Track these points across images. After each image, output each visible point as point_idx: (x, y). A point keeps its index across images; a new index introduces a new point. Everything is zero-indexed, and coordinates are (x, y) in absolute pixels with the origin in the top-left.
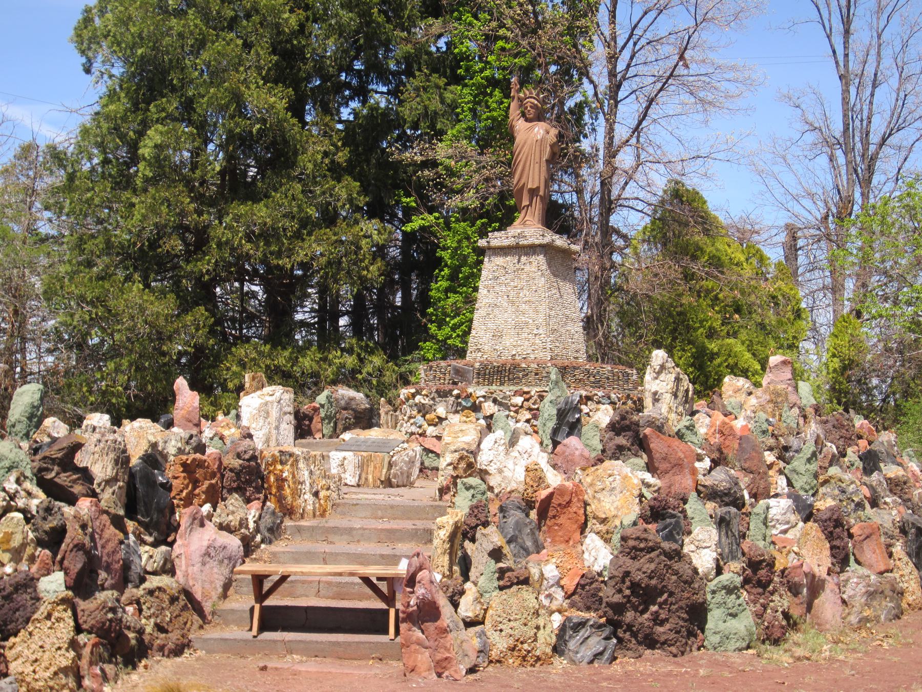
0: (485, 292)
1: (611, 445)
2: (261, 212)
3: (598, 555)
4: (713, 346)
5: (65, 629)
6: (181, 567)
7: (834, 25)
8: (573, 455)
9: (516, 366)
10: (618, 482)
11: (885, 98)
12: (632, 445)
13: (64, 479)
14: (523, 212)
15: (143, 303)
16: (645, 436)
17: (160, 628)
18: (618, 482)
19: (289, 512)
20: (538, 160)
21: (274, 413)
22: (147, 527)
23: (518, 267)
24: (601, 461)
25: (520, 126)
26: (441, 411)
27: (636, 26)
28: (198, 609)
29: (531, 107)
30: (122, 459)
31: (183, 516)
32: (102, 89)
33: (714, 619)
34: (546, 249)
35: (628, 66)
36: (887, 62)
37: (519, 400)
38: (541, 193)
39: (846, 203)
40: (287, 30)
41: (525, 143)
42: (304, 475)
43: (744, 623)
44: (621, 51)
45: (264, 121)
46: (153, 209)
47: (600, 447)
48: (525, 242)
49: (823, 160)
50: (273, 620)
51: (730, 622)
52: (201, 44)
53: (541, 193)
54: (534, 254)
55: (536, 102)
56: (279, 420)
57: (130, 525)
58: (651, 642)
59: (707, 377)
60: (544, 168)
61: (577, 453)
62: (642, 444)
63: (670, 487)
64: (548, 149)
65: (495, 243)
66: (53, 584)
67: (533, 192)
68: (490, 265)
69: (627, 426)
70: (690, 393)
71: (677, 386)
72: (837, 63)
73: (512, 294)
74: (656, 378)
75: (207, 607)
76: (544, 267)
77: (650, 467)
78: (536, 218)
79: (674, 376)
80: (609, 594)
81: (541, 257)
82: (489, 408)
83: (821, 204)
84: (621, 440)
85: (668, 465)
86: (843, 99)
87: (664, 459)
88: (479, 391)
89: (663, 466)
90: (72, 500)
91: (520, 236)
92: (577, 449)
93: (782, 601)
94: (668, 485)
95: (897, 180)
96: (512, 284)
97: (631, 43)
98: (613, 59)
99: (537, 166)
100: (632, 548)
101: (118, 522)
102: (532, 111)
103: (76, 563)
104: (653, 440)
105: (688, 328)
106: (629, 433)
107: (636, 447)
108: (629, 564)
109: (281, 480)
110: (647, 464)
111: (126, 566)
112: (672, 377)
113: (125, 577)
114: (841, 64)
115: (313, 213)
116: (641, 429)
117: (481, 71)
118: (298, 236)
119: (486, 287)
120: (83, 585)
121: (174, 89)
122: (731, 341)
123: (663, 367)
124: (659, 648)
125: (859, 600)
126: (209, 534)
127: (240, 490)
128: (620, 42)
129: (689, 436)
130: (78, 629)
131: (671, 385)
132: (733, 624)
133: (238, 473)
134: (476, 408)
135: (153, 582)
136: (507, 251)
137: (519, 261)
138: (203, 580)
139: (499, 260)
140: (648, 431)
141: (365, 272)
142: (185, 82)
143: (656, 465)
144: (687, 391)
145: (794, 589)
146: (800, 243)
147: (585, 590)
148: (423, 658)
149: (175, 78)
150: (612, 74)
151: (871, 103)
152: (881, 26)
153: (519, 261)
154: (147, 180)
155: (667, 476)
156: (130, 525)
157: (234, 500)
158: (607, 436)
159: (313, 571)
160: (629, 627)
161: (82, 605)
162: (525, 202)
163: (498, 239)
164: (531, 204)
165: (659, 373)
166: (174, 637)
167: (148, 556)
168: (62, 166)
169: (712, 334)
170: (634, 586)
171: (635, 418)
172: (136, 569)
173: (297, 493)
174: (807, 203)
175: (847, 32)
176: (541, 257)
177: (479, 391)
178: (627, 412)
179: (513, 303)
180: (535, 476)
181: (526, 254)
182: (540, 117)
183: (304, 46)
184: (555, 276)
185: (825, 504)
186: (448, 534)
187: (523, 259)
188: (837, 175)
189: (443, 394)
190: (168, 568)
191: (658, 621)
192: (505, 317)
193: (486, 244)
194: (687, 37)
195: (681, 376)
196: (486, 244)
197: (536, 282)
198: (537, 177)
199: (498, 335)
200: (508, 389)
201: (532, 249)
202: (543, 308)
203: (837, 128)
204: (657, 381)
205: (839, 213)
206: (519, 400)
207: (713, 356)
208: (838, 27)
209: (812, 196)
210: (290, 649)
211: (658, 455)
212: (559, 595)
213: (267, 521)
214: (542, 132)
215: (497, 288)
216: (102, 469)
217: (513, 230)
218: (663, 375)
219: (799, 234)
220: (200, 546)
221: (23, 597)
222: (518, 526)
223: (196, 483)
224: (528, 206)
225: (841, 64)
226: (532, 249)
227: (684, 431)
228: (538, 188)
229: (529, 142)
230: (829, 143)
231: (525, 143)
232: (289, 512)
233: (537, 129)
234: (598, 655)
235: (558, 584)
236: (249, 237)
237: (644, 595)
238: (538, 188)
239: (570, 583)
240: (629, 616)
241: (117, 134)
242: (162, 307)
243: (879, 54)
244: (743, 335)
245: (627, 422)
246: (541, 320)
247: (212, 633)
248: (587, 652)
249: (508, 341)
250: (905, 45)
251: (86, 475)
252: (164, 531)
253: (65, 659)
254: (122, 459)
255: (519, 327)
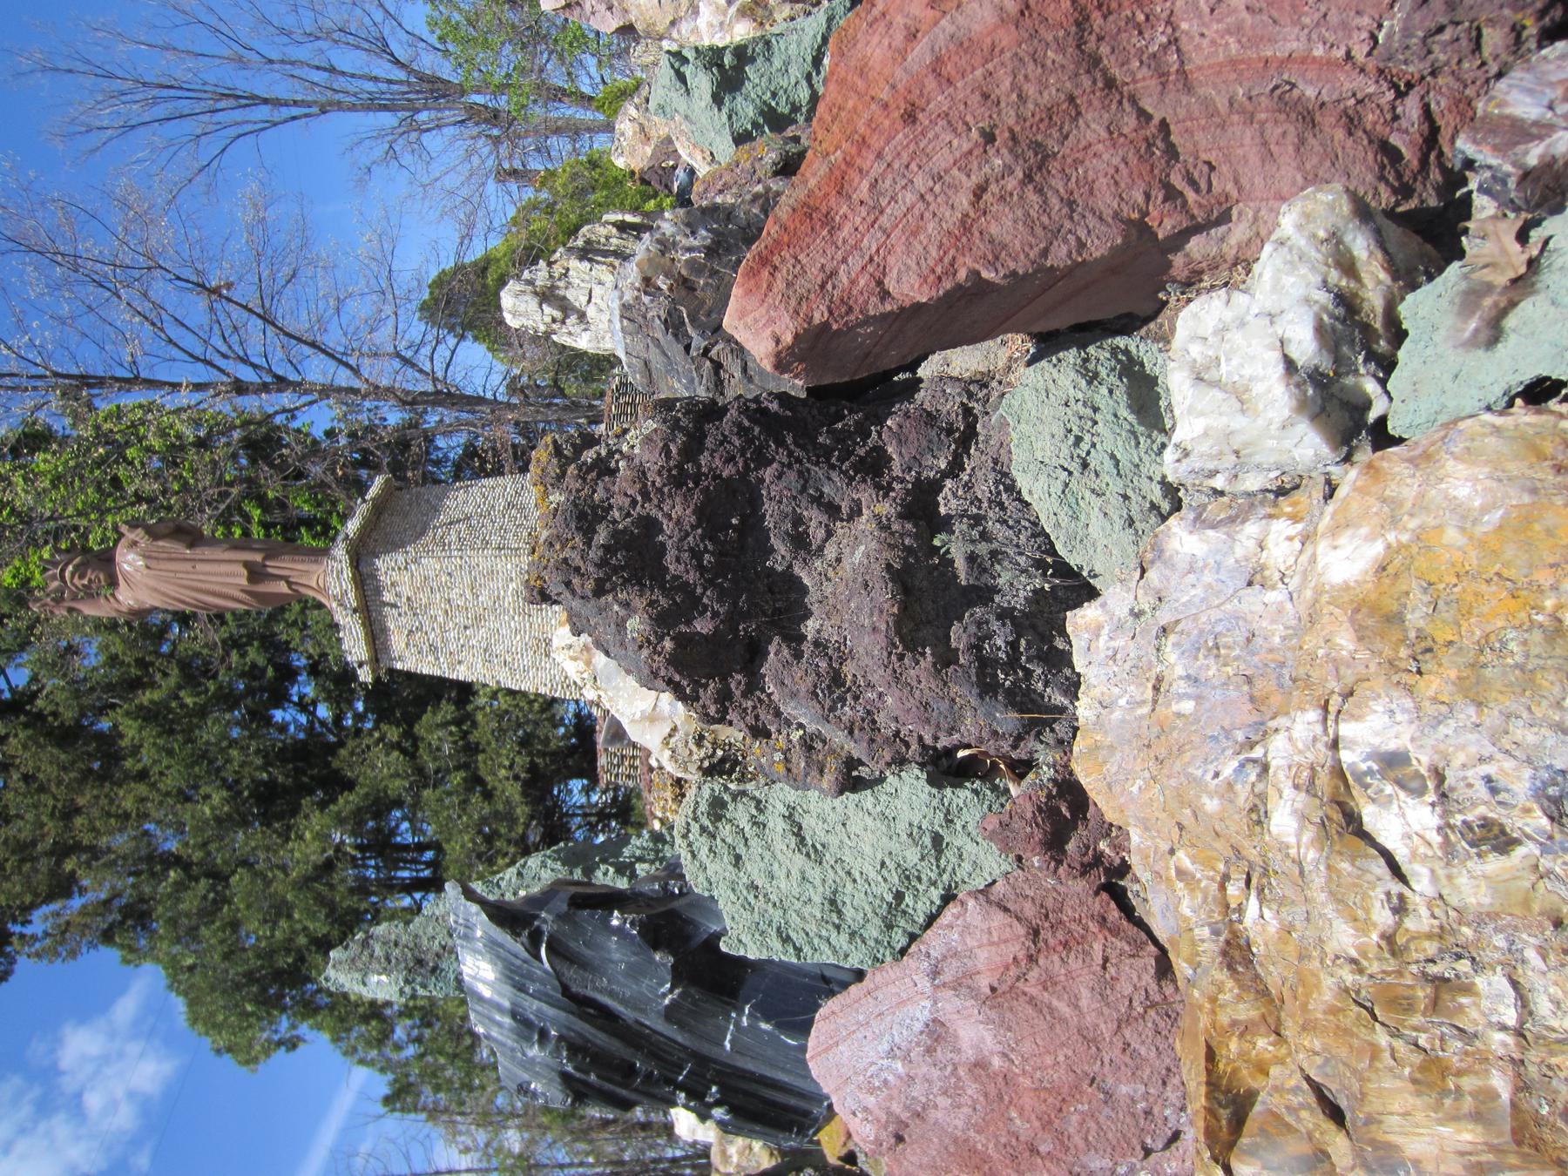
0: (462, 668)
1: (901, 697)
8: (998, 1088)
10: (1462, 744)
11: (348, 60)
12: (874, 467)
14: (303, 590)
16: (810, 346)
18: (1462, 744)
20: (188, 566)
23: (405, 608)
24: (1067, 808)
25: (127, 598)
27: (191, 355)
29: (82, 577)
36: (302, 53)
38: (258, 557)
39: (473, 113)
40: (226, 809)
41: (156, 590)
44: (228, 375)
47: (910, 794)
48: (352, 595)
53: (258, 557)
54: (375, 577)
55: (70, 568)
60: (207, 552)
61: (974, 1033)
62: (852, 391)
63: (1308, 118)
64: (161, 543)
67: (256, 574)
68: (409, 658)
69: (709, 518)
70: (629, 218)
71: (606, 254)
72: (306, 116)
73: (461, 620)
74: (582, 316)
76: (401, 558)
77: (1105, 304)
78: (313, 567)
79: (574, 263)
81: (379, 563)
84: (845, 571)
85: (1093, 127)
86: (349, 109)
87: (1037, 164)
89: (1106, 179)
92: (937, 1032)
94: (1283, 131)
96: (440, 619)
97: (221, 362)
98: (240, 388)
99: (200, 567)
102: (90, 574)
104: (852, 275)
106: (777, 492)
107: (893, 435)
110: (1047, 344)
112: (578, 267)
114: (307, 111)
116: (735, 387)
118: (488, 795)
119: (452, 667)
123: (547, 296)
128: (214, 376)
129: (781, 76)
131: (601, 272)
136: (376, 627)
137: (394, 606)
139: (397, 642)
140: (757, 327)
141: (536, 705)
142: (287, 946)
143: (1100, 243)
144: (622, 227)
146: (517, 165)
150: (265, 387)
151: (353, 76)
152: (258, 58)
153: (394, 606)
155: (1195, 142)
158: (804, 715)
164: (286, 579)
165: (565, 307)
171: (639, 441)
176: (379, 563)
178: (585, 517)
179: (478, 619)
181: (378, 591)
182: (106, 560)
183: (253, 781)
184: (423, 533)
187: (388, 597)
193: (366, 668)
194: (178, 283)
195: (580, 243)
196: (366, 668)
197: (432, 574)
198: (224, 568)
201: (365, 582)
202: (483, 560)
203: (387, 119)
204: (591, 312)
205: (486, 121)
208: (263, 112)
211: (1003, 225)
214: (131, 557)
215: (453, 647)
218: (570, 295)
219: (506, 166)
224: (289, 584)
225: (307, 111)
226: (365, 582)
227: (746, 109)
228: (246, 564)
229: (153, 583)
231: (156, 590)
233: (126, 566)
238: (246, 564)
243: (293, 63)
245: (676, 516)
250: (283, 32)
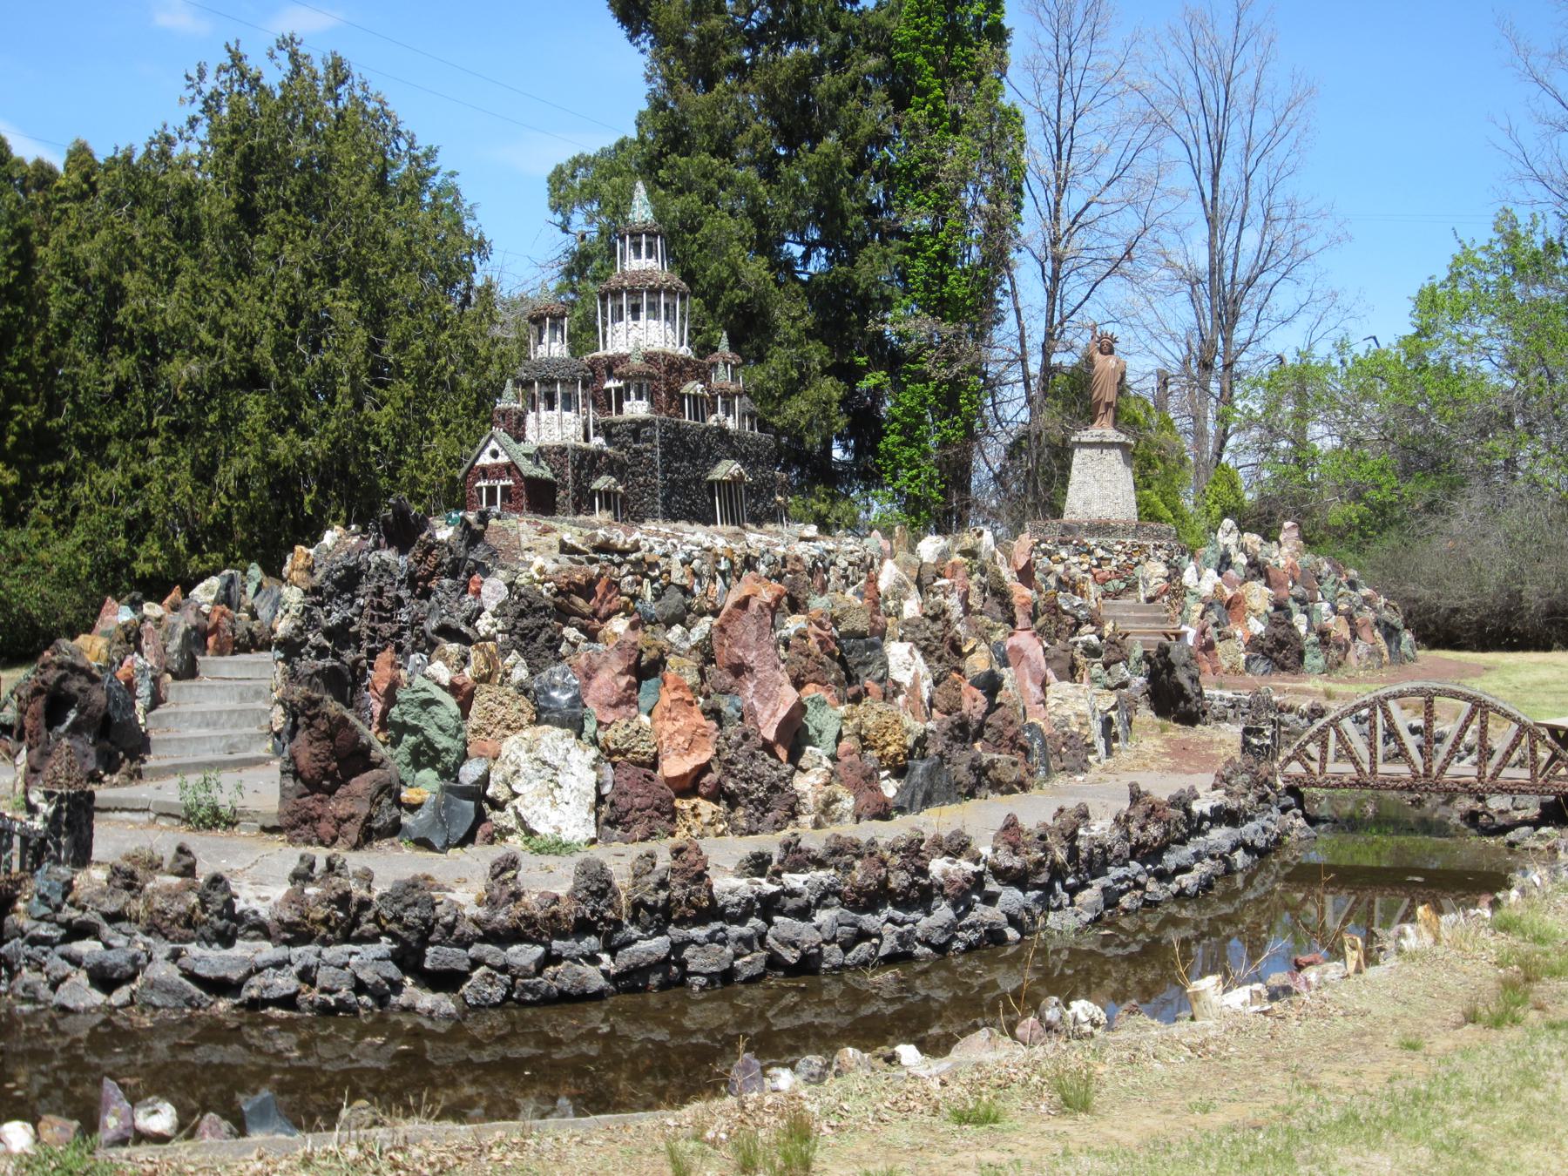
3: (1257, 627)
7: (1203, 164)
9: (1107, 524)
11: (1251, 239)
26: (1064, 554)
33: (1308, 658)
37: (1119, 547)
39: (1208, 346)
43: (1320, 662)
49: (1183, 296)
51: (1314, 660)
58: (1283, 668)
65: (1084, 439)
67: (1108, 405)
68: (1079, 457)
77: (1268, 585)
82: (1100, 553)
83: (1184, 347)
88: (1092, 542)
91: (1102, 435)
93: (1334, 652)
100: (1273, 622)
117: (933, 245)
122: (1147, 492)
124: (336, 1074)
125: (1365, 657)
132: (1316, 662)
134: (1090, 553)
139: (1087, 451)
145: (1339, 647)
147: (1253, 643)
162: (1102, 411)
163: (1087, 436)
170: (1278, 640)
174: (1170, 345)
175: (1215, 176)
177: (1092, 542)
185: (1343, 607)
188: (1199, 316)
189: (1064, 543)
192: (1093, 490)
200: (1111, 541)
201: (1112, 445)
206: (1119, 547)
209: (1173, 337)
226: (1112, 445)
230: (1195, 282)
237: (1281, 644)
249: (1095, 507)
255: (1104, 498)
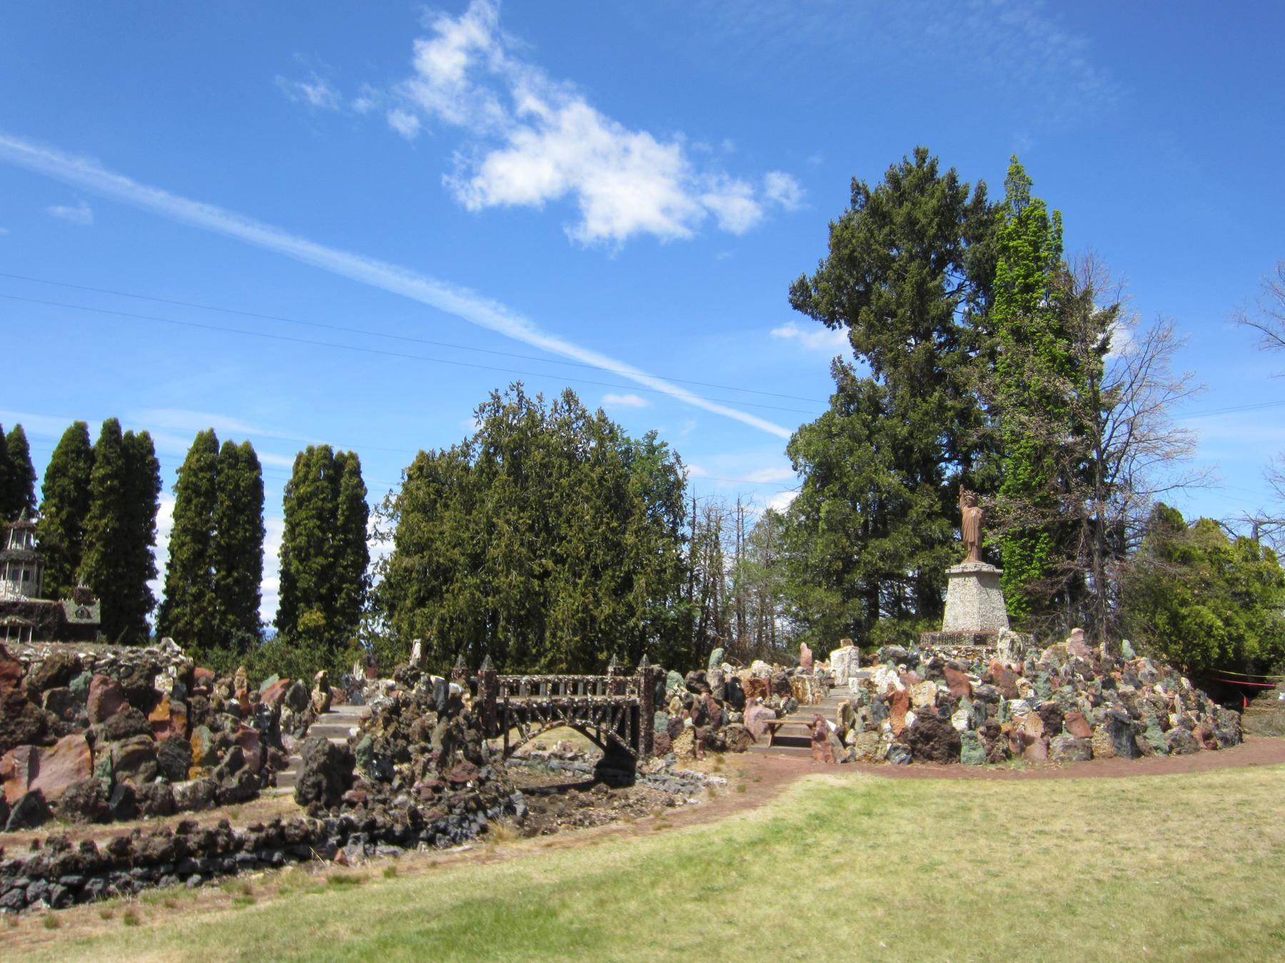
2: (887, 544)
4: (1184, 611)
5: (691, 737)
6: (746, 720)
13: (698, 686)
15: (828, 598)
17: (734, 742)
19: (801, 701)
21: (847, 659)
22: (733, 705)
25: (965, 509)
28: (752, 736)
30: (722, 679)
31: (748, 701)
32: (804, 477)
33: (964, 750)
34: (979, 574)
35: (1111, 437)
37: (955, 652)
42: (808, 686)
43: (980, 752)
45: (889, 493)
46: (827, 546)
50: (776, 741)
52: (851, 452)
56: (850, 663)
57: (725, 704)
58: (930, 758)
59: (1180, 632)
66: (688, 722)
67: (972, 544)
68: (952, 582)
75: (756, 736)
80: (911, 737)
84: (935, 672)
90: (699, 693)
95: (92, 769)
98: (1114, 429)
101: (718, 702)
103: (696, 714)
105: (1166, 600)
108: (919, 724)
109: (797, 689)
111: (721, 718)
113: (720, 722)
115: (918, 541)
120: (699, 722)
121: (837, 479)
122: (1199, 607)
126: (760, 708)
127: (778, 692)
130: (696, 737)
132: (973, 753)
133: (777, 685)
135: (733, 725)
138: (756, 727)
139: (956, 580)
148: (820, 755)
149: (836, 473)
154: (823, 531)
156: (725, 704)
157: (776, 697)
159: (794, 725)
160: (919, 751)
161: (698, 729)
163: (956, 569)
166: (740, 746)
167: (732, 715)
168: (782, 524)
169: (1184, 603)
170: (921, 733)
172: (725, 720)
173: (805, 694)
180: (891, 687)
186: (66, 611)
190: (741, 720)
191: (933, 748)
199: (956, 619)
201: (970, 574)
202: (977, 605)
206: (955, 652)
207: (1184, 618)
210: (781, 752)
212: (891, 736)
213: (790, 704)
216: (713, 682)
217: (962, 565)
220: (755, 713)
221: (679, 726)
222: (878, 708)
223: (755, 689)
226: (970, 574)
232: (801, 701)
234: (902, 761)
235: (891, 731)
236: (881, 558)
237: (927, 738)
239: (898, 731)
240: (919, 746)
241: (807, 503)
242: (834, 599)
244: (1211, 603)
246: (975, 610)
247: (756, 746)
248: (897, 759)
249: (960, 622)
251: (707, 685)
252: (740, 706)
253: (690, 747)
254: (722, 679)
255: (965, 614)
